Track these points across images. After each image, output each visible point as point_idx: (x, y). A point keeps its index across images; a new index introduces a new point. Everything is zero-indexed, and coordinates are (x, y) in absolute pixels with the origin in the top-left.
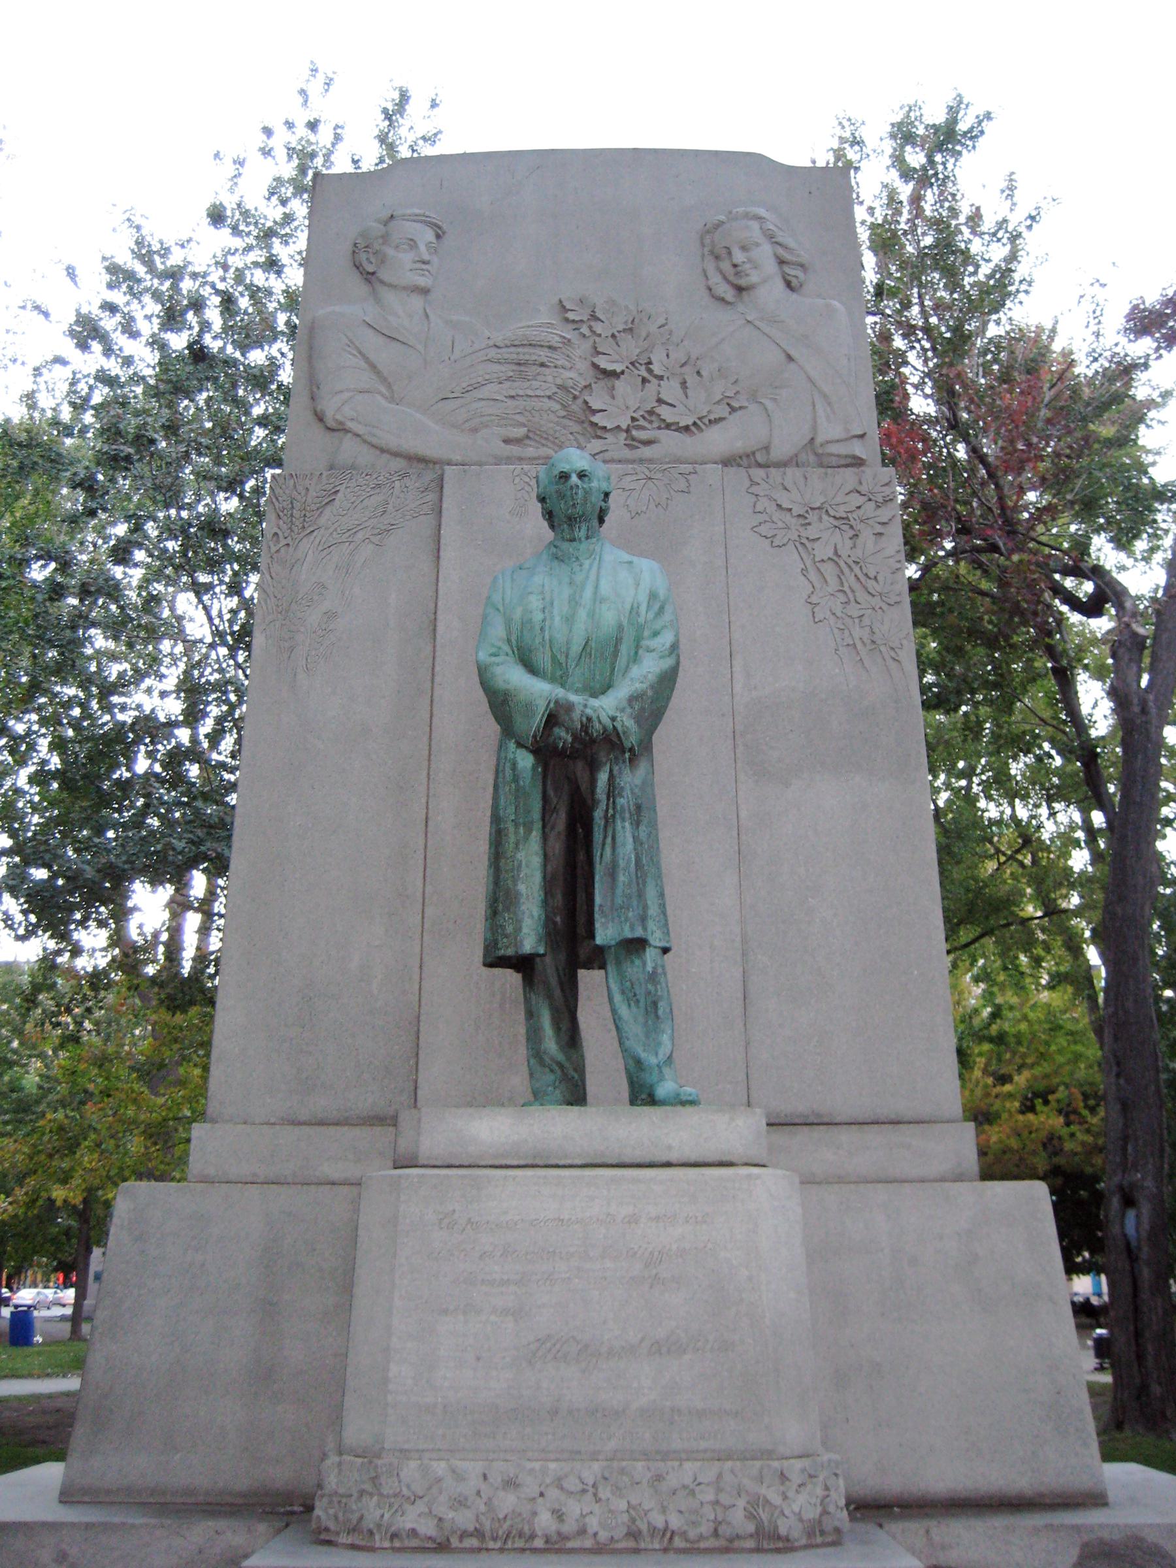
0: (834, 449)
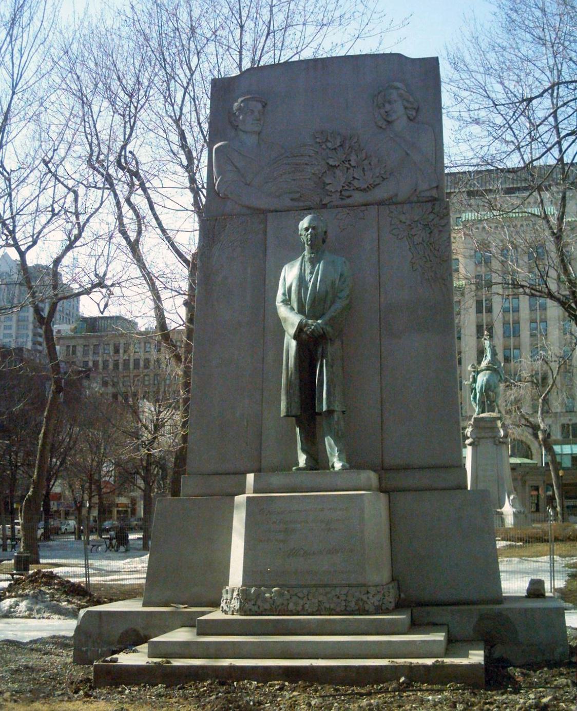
0: (423, 194)
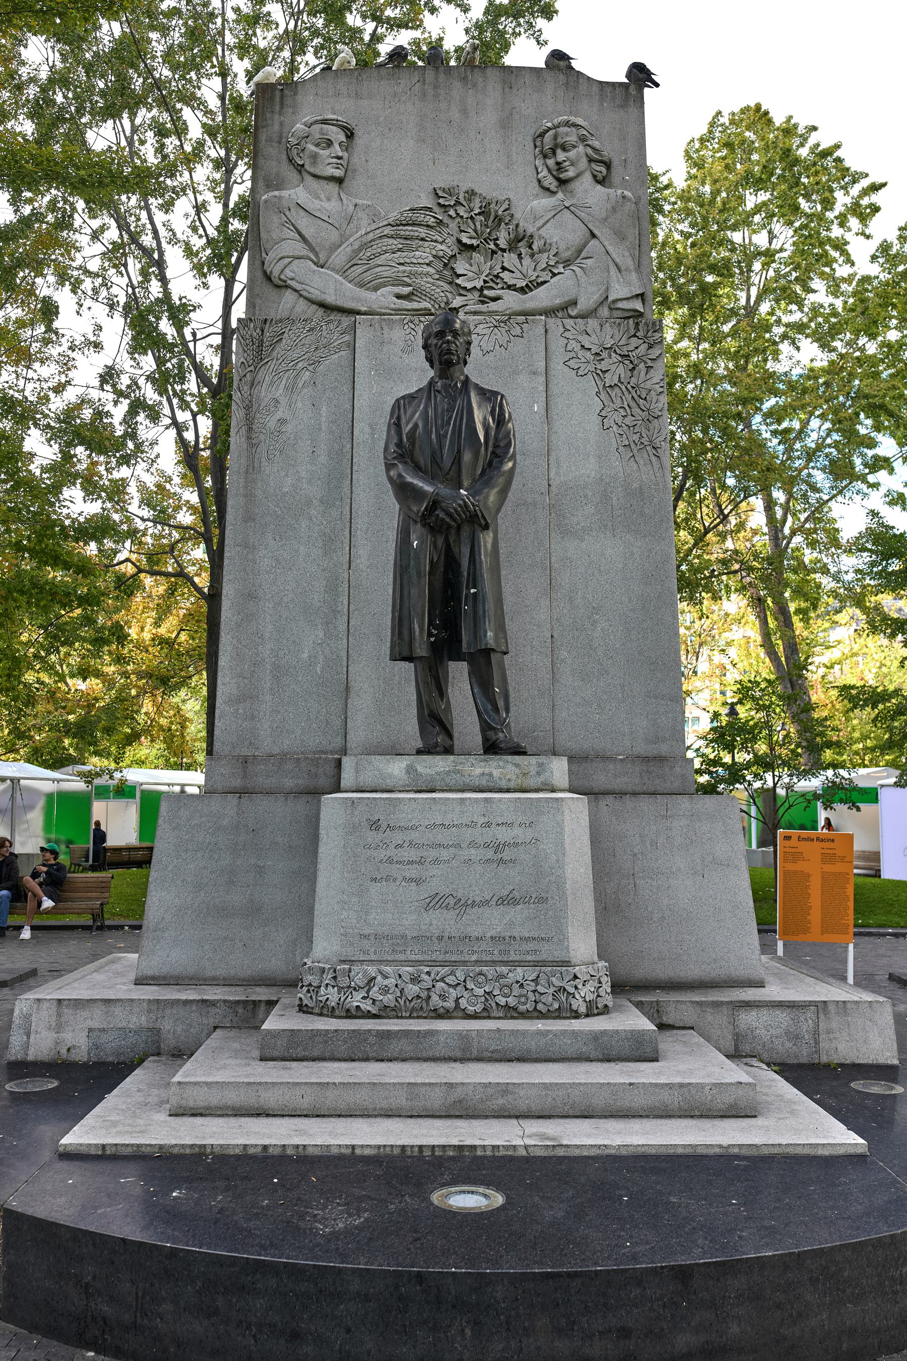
0: (620, 305)
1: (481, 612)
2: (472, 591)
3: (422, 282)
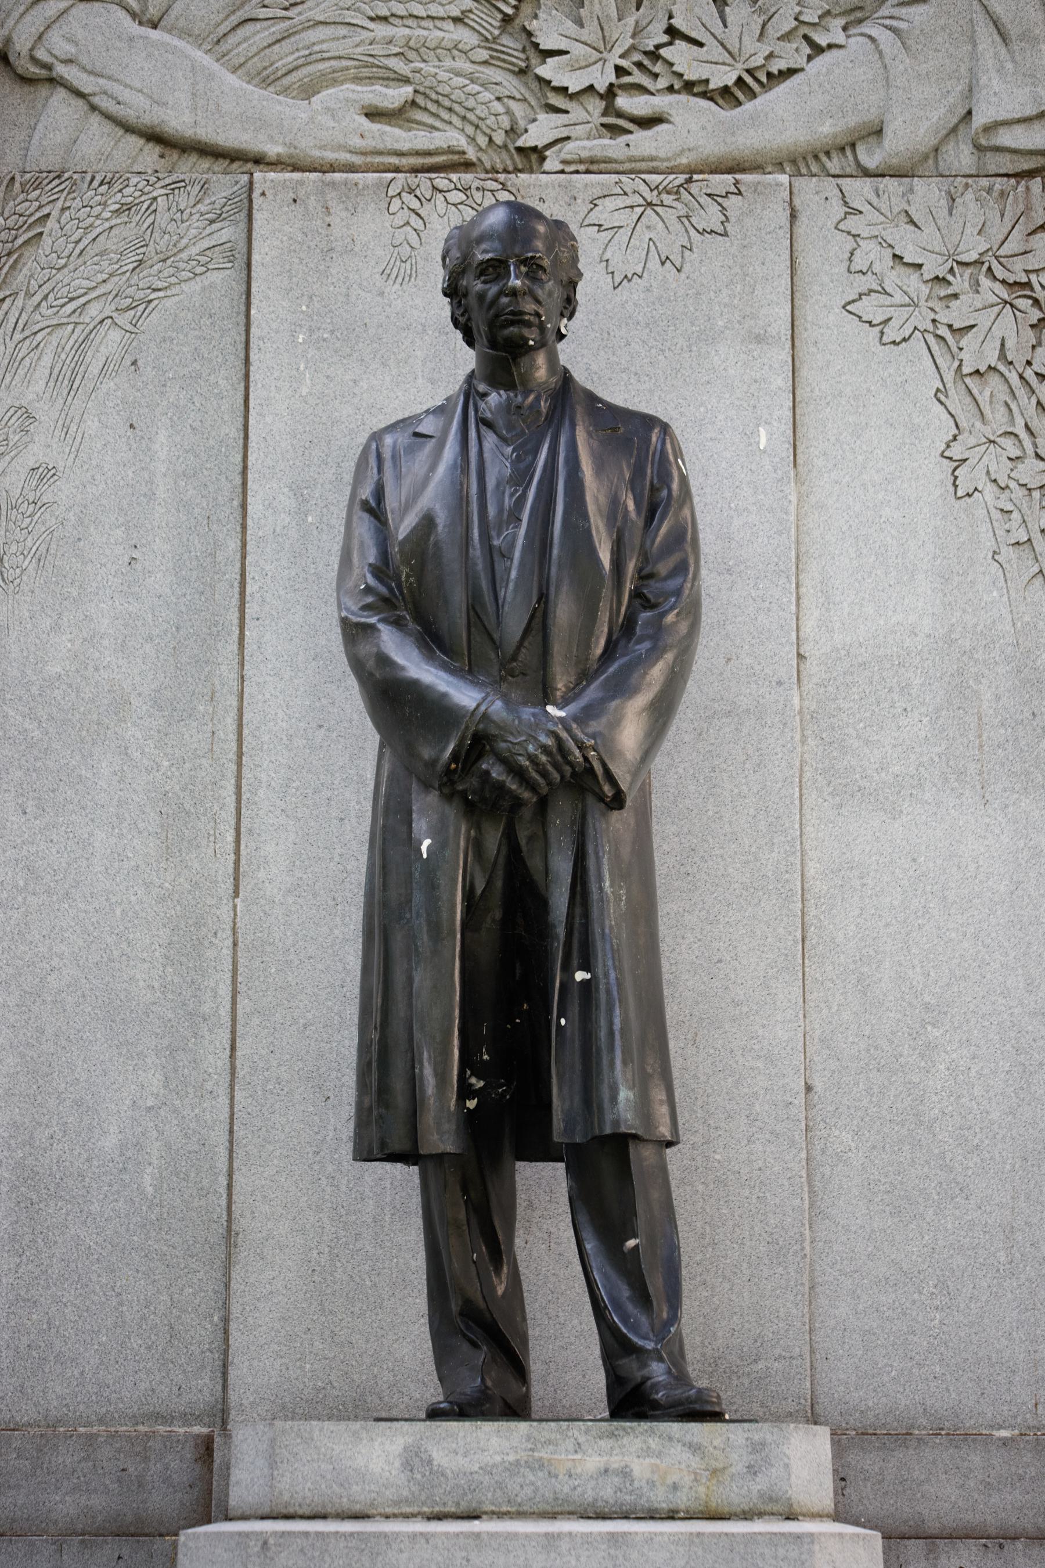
0: (1006, 138)
1: (603, 1034)
2: (580, 976)
3: (441, 72)
